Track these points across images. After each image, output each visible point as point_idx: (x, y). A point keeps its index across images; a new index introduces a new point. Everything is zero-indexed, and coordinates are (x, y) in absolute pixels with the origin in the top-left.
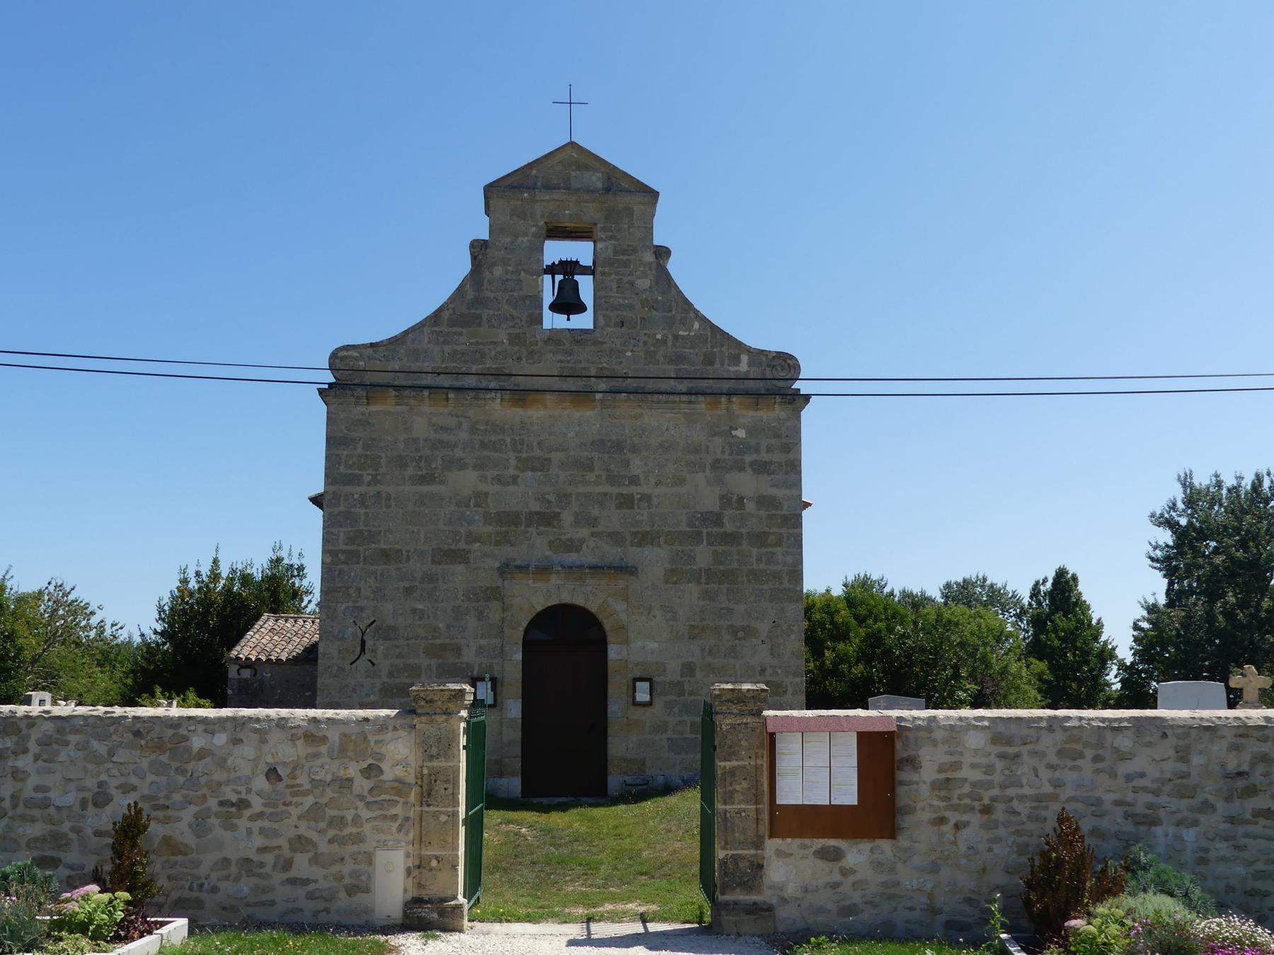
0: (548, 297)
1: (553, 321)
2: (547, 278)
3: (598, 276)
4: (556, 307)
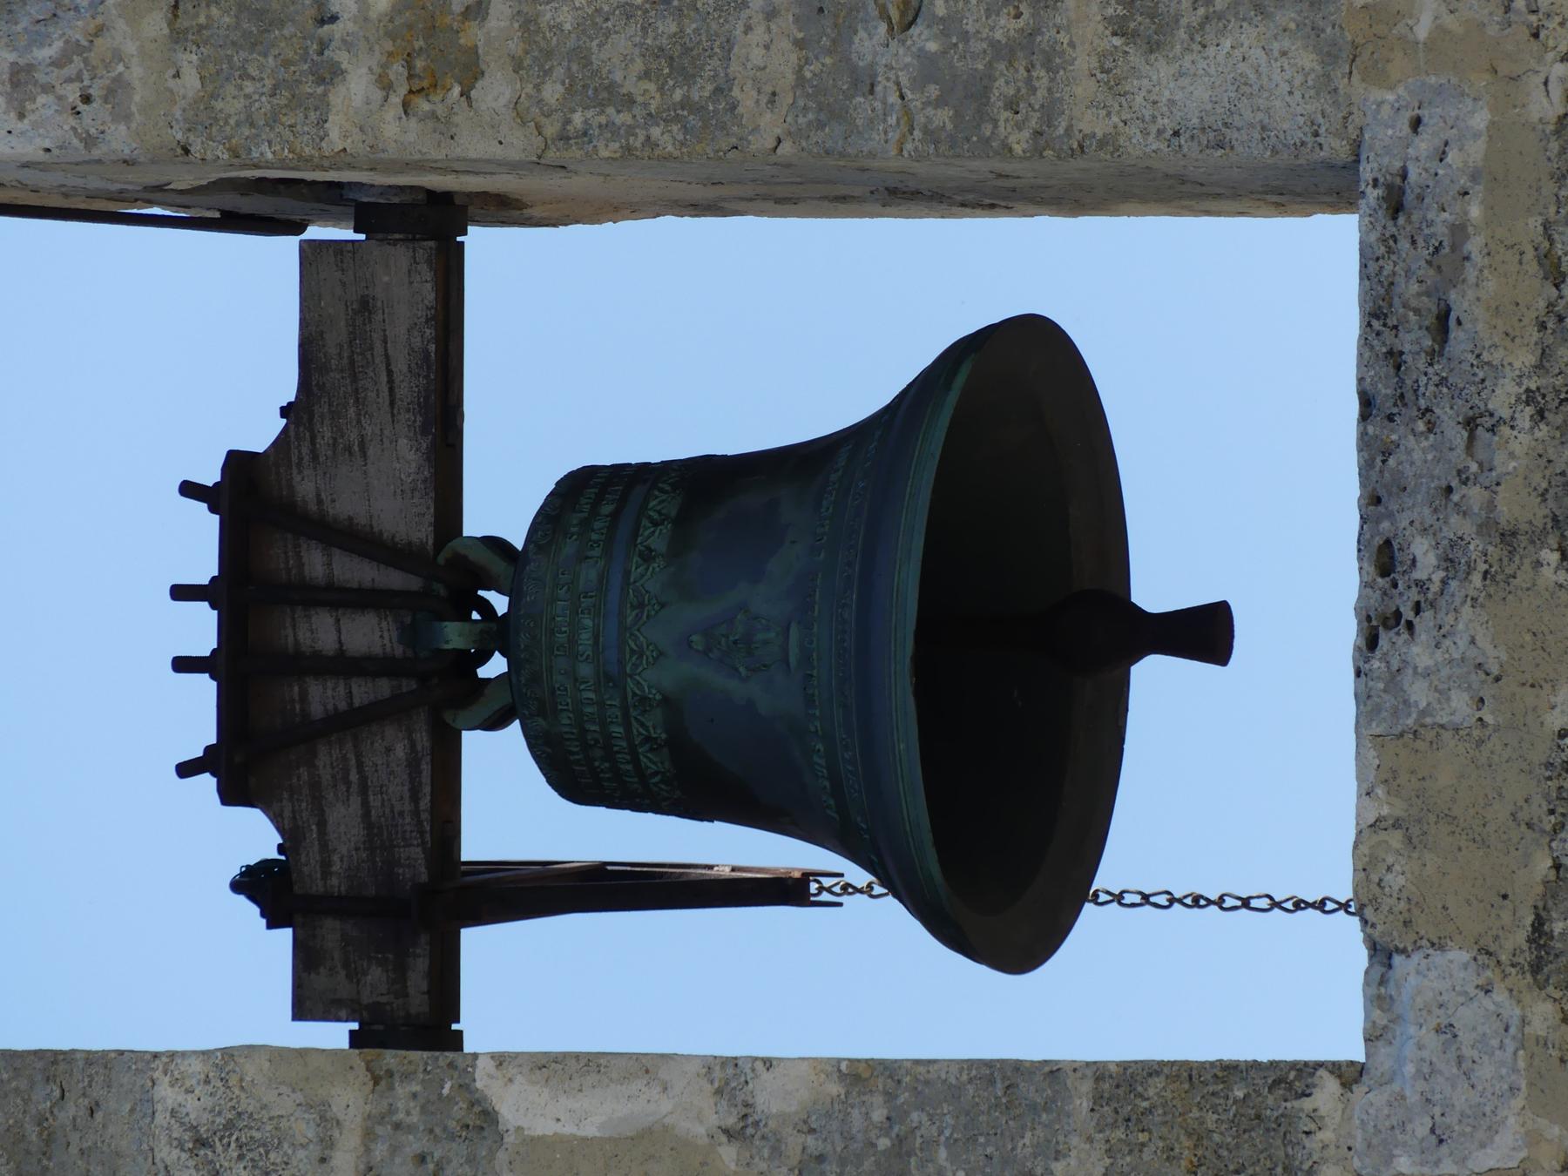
0: (845, 977)
1: (1238, 869)
2: (518, 987)
3: (482, 134)
4: (1003, 849)
